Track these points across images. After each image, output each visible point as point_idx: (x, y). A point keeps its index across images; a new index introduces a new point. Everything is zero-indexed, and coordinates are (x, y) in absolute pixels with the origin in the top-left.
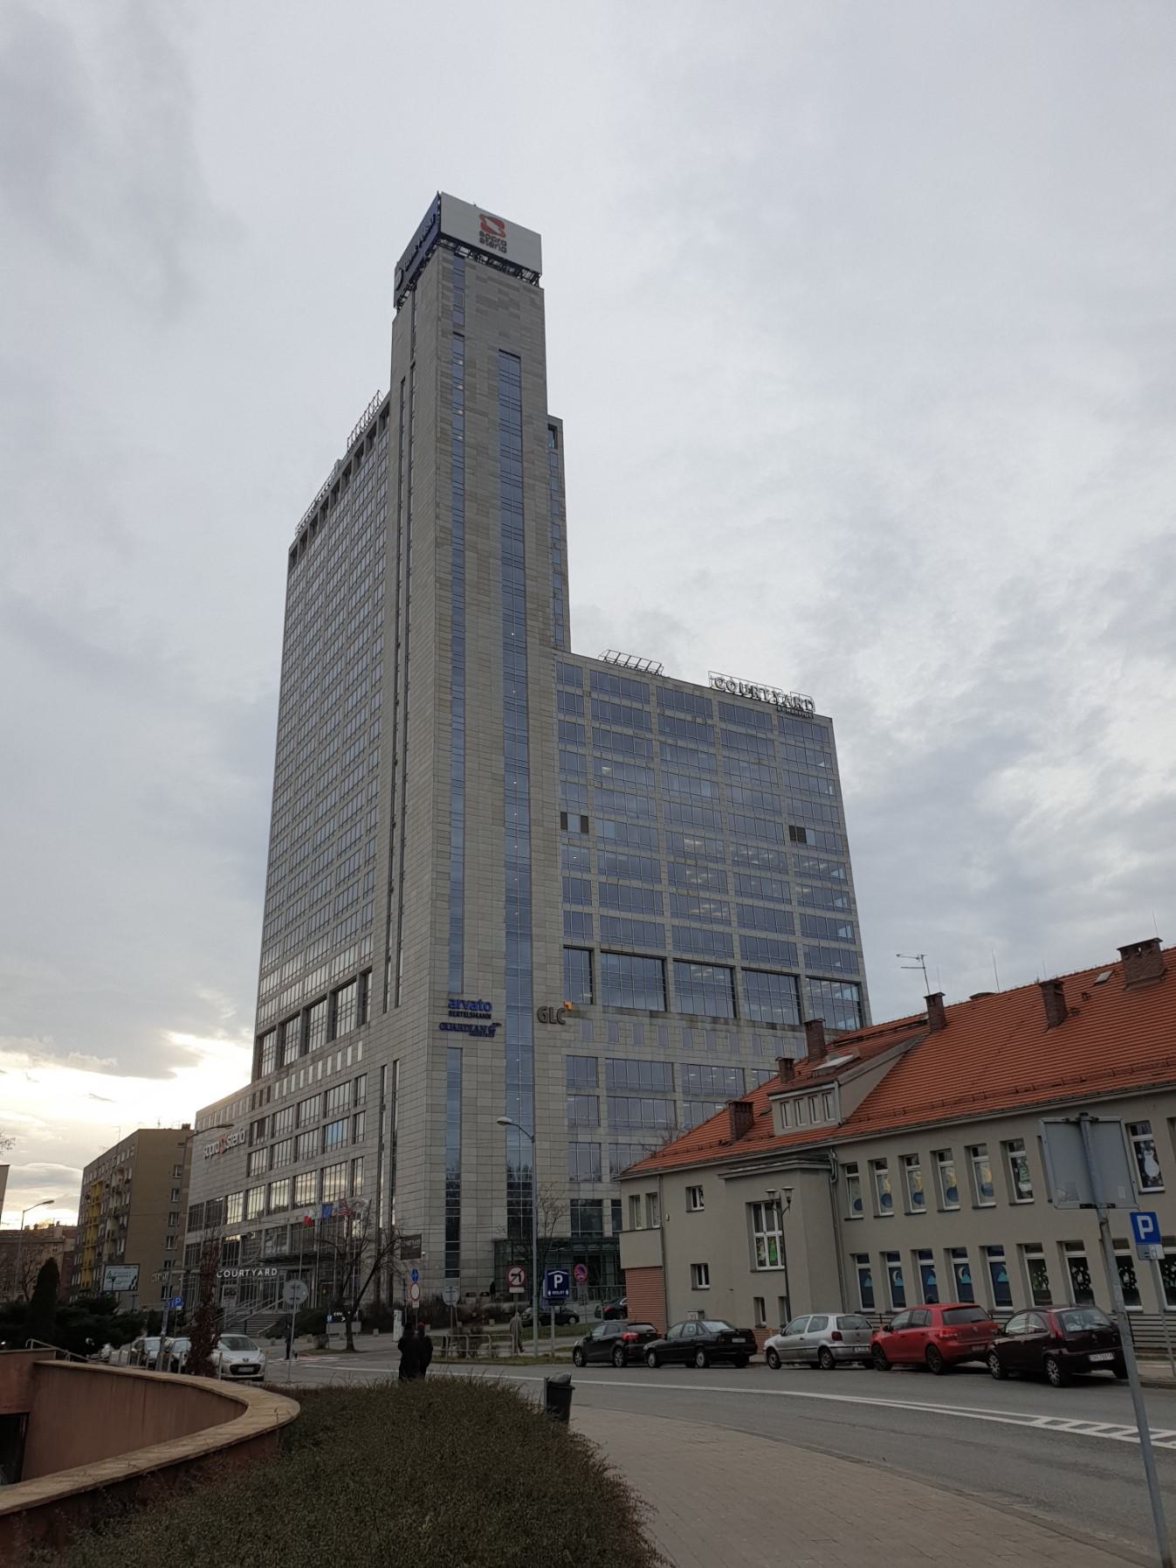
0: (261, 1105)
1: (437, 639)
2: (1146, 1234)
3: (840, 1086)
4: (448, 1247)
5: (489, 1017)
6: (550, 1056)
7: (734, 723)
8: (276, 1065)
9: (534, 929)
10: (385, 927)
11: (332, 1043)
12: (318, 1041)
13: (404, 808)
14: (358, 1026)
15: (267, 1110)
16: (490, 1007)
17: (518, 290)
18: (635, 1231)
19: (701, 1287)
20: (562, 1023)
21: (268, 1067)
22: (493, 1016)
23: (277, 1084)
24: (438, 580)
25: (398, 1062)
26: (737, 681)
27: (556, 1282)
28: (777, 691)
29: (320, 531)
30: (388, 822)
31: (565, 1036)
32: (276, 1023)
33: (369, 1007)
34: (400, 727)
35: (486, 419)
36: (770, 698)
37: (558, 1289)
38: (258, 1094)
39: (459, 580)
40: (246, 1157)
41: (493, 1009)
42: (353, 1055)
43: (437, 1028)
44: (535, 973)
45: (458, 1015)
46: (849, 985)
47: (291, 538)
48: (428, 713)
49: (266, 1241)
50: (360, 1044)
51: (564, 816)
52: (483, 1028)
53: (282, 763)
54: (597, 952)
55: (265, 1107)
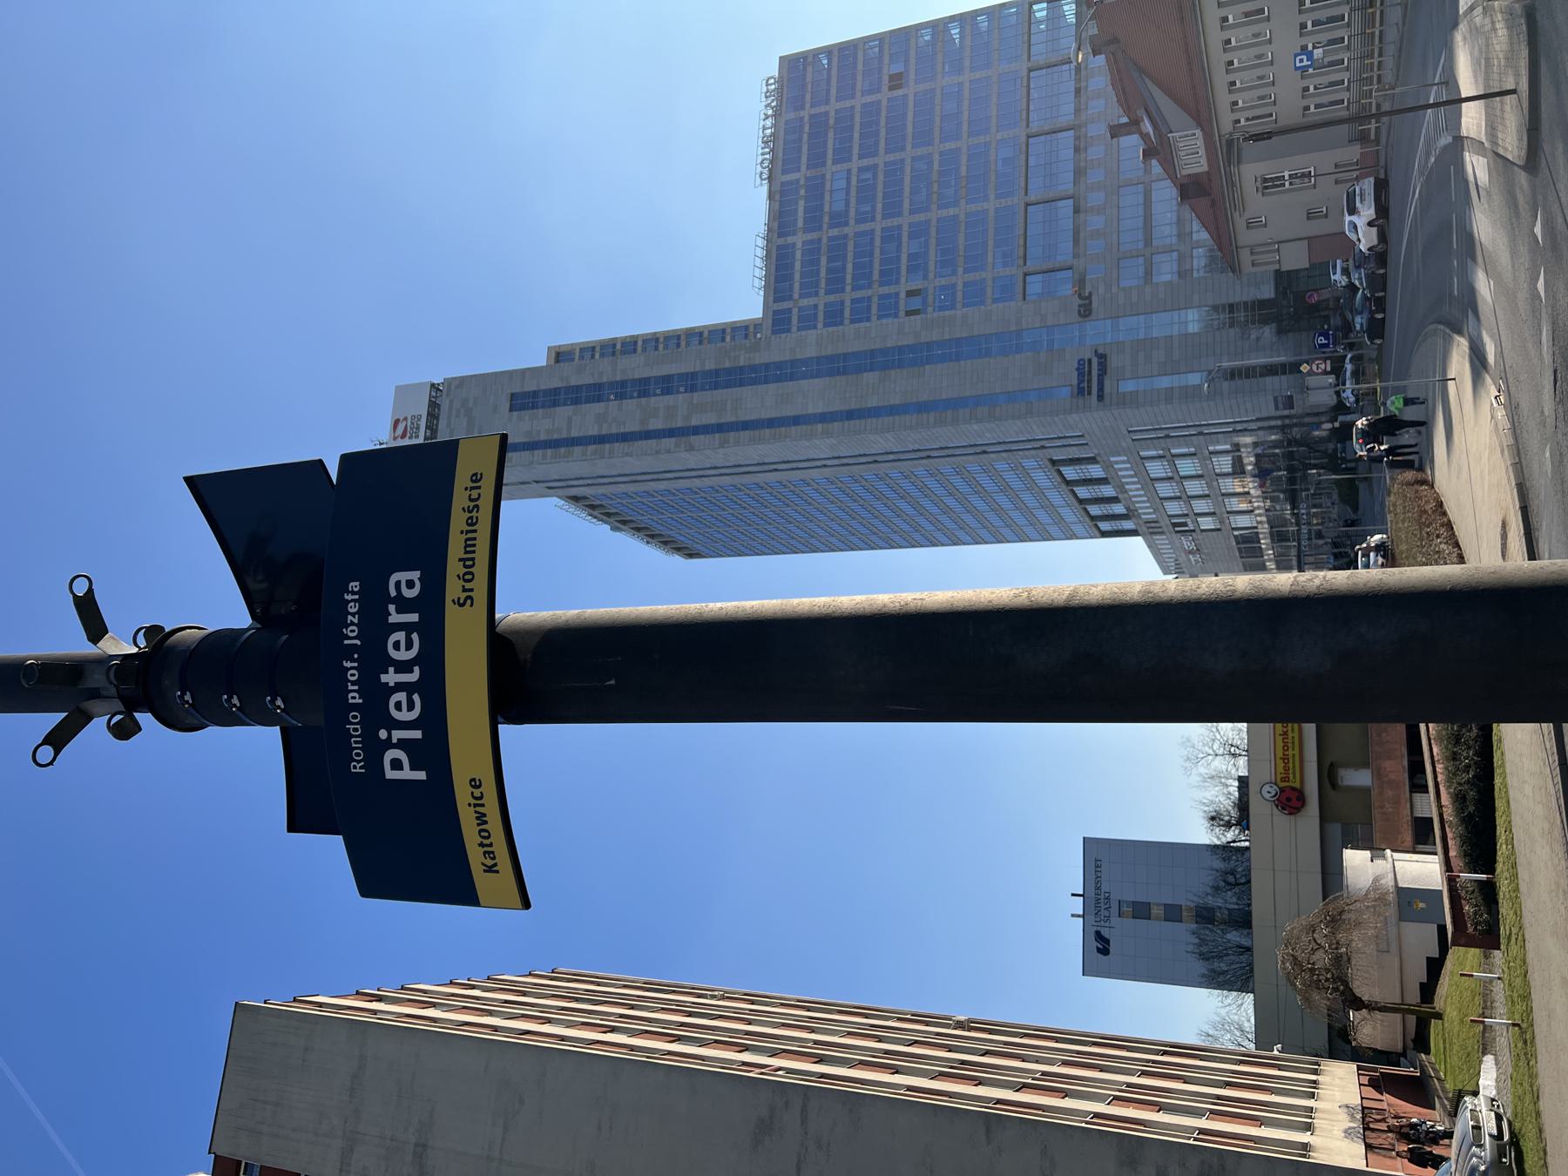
0: (1160, 527)
1: (772, 441)
2: (1307, 61)
3: (1171, 132)
4: (1284, 373)
5: (1090, 360)
6: (1120, 302)
7: (800, 158)
8: (1126, 519)
9: (1011, 329)
10: (1015, 453)
11: (1110, 480)
12: (1107, 491)
13: (915, 451)
14: (1097, 462)
15: (1165, 522)
16: (1081, 360)
17: (451, 402)
18: (1279, 260)
19: (1325, 212)
20: (1090, 294)
21: (1128, 525)
22: (1090, 357)
23: (1143, 516)
24: (722, 446)
25: (1130, 429)
26: (760, 158)
27: (1324, 341)
28: (763, 117)
29: (669, 536)
30: (925, 461)
31: (1101, 290)
32: (1091, 524)
33: (1082, 456)
34: (845, 461)
35: (574, 417)
36: (769, 123)
37: (1328, 340)
38: (1151, 530)
39: (720, 428)
40: (1203, 533)
41: (1082, 357)
42: (1121, 464)
43: (1102, 404)
44: (1049, 323)
45: (1089, 387)
46: (1032, 15)
47: (677, 560)
48: (834, 442)
49: (1276, 510)
50: (1112, 459)
51: (909, 313)
52: (1100, 364)
53: (779, 499)
54: (1026, 269)
55: (1162, 524)
